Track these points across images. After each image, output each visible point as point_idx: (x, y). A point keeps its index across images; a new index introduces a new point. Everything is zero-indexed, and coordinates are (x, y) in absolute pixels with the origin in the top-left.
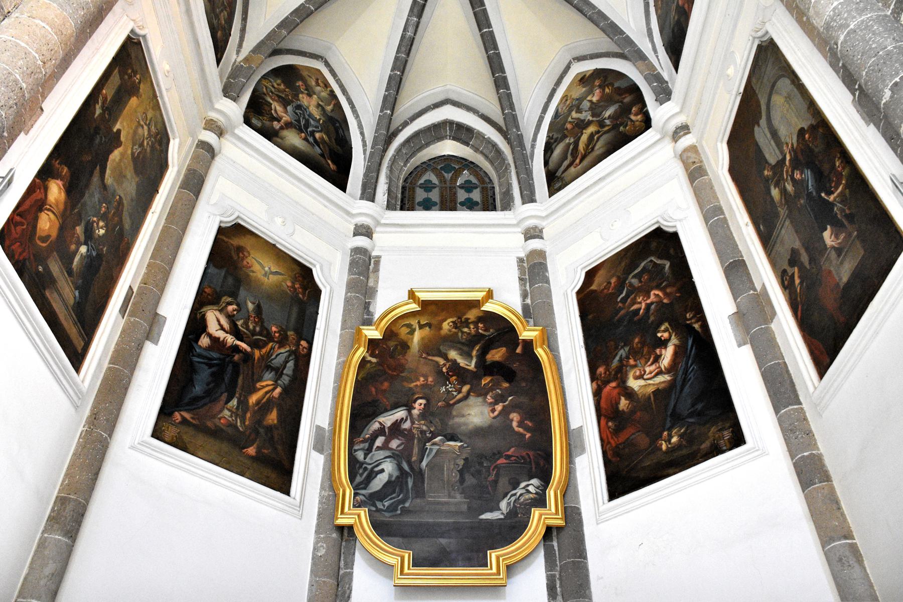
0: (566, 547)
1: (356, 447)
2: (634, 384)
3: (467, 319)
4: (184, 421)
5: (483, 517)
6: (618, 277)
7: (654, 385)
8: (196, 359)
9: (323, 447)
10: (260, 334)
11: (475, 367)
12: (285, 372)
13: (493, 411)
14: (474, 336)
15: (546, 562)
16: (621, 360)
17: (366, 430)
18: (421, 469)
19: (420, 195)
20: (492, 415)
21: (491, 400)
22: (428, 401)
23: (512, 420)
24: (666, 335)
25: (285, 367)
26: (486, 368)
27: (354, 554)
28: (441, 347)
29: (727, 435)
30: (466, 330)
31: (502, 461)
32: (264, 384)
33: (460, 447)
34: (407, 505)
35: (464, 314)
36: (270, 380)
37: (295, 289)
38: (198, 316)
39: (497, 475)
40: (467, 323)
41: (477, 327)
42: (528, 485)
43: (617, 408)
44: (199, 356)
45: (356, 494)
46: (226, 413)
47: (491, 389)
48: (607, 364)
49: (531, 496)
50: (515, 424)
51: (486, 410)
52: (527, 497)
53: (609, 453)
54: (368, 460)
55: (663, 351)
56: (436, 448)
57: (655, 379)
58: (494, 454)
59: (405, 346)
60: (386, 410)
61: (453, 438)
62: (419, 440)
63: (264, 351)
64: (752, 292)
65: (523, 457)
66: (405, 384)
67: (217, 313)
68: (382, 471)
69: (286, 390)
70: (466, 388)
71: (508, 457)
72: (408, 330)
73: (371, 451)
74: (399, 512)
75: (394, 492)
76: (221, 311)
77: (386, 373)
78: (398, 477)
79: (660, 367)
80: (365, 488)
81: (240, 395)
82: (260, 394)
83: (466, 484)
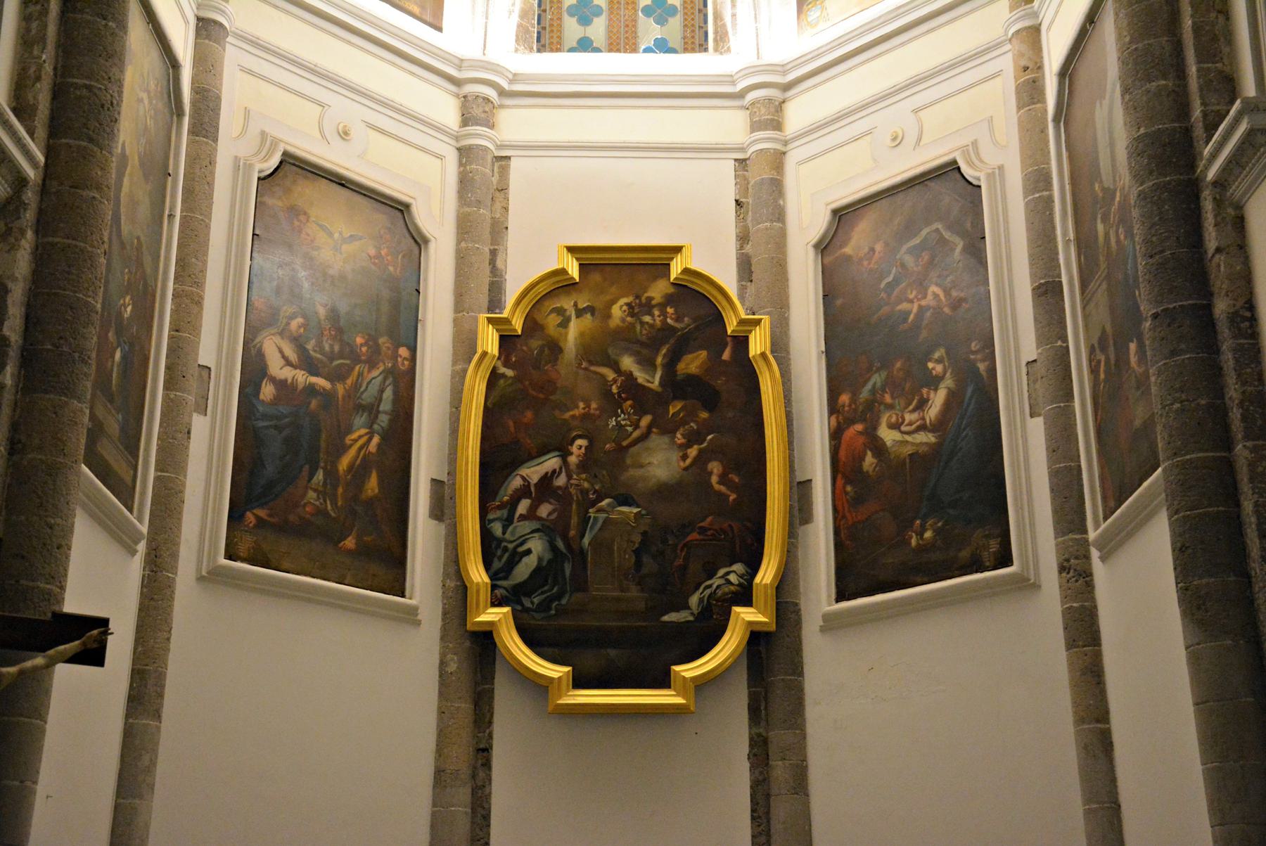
0: (771, 657)
1: (491, 516)
2: (888, 436)
3: (650, 299)
4: (261, 523)
5: (666, 618)
6: (887, 244)
7: (913, 444)
9: (442, 512)
10: (341, 356)
11: (661, 384)
13: (684, 457)
16: (873, 391)
19: (572, 29)
21: (683, 441)
23: (711, 473)
24: (939, 368)
25: (381, 400)
26: (676, 386)
28: (610, 351)
29: (994, 545)
30: (647, 319)
31: (695, 536)
32: (354, 436)
34: (564, 601)
35: (645, 290)
38: (253, 352)
39: (686, 559)
40: (648, 307)
42: (728, 573)
44: (265, 417)
45: (494, 587)
46: (312, 495)
47: (683, 422)
48: (855, 395)
49: (732, 588)
50: (714, 479)
51: (675, 456)
52: (726, 590)
54: (507, 536)
55: (932, 395)
56: (603, 516)
57: (916, 435)
58: (684, 526)
59: (555, 348)
60: (531, 457)
61: (626, 501)
62: (578, 503)
63: (349, 382)
64: (1059, 343)
65: (725, 532)
66: (557, 413)
67: (278, 339)
68: (529, 552)
69: (385, 437)
70: (646, 421)
71: (703, 530)
73: (512, 523)
76: (281, 334)
78: (550, 562)
79: (923, 419)
80: (506, 578)
81: (326, 463)
82: (352, 452)
83: (645, 571)
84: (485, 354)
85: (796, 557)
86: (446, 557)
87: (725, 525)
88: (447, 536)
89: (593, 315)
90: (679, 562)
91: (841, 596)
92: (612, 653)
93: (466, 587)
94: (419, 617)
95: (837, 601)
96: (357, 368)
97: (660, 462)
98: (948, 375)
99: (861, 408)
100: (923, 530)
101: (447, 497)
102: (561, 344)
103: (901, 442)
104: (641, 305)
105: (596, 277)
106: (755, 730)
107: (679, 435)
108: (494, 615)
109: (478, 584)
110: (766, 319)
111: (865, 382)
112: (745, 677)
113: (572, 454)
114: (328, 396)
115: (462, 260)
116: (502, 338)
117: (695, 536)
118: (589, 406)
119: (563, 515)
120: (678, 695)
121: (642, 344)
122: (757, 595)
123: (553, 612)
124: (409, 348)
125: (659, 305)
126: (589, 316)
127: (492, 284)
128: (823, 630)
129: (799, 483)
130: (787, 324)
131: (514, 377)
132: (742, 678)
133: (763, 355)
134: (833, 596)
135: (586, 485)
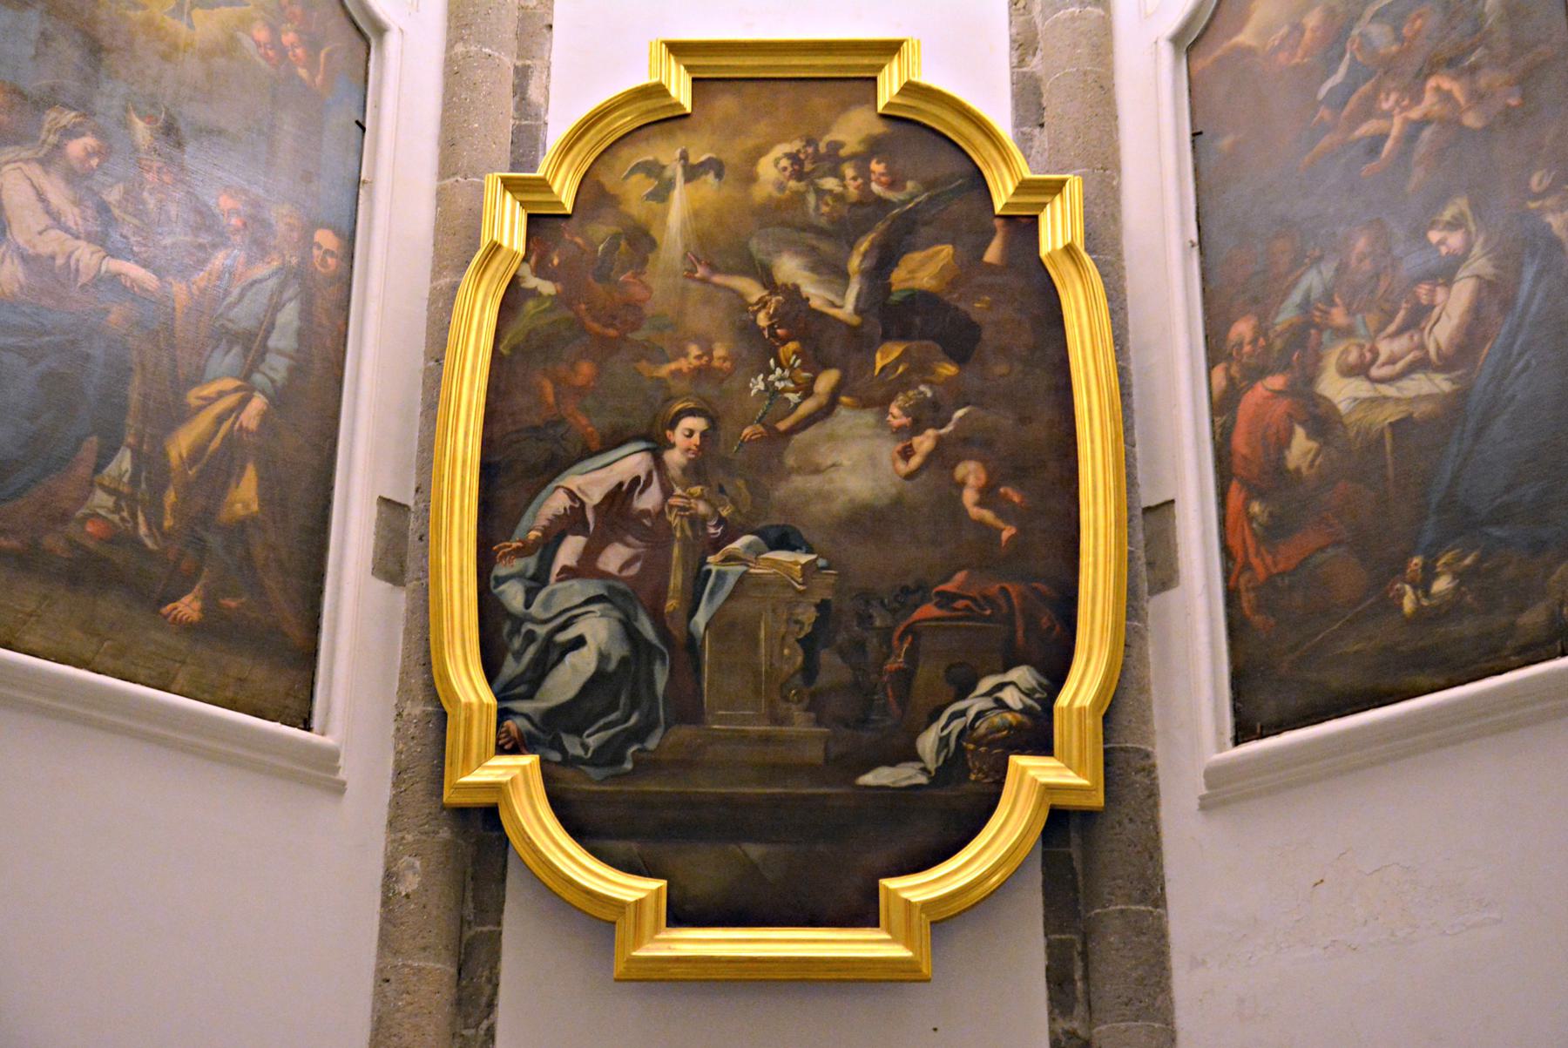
1: (501, 570)
2: (1338, 390)
3: (836, 146)
5: (868, 779)
7: (1398, 400)
9: (402, 564)
11: (858, 311)
12: (271, 343)
13: (907, 453)
14: (859, 204)
15: (1048, 904)
18: (691, 637)
20: (903, 468)
21: (904, 421)
22: (713, 422)
23: (961, 485)
26: (893, 314)
27: (503, 879)
28: (755, 245)
30: (830, 183)
31: (929, 610)
32: (209, 390)
33: (804, 566)
34: (652, 743)
35: (827, 129)
37: (282, 52)
39: (912, 655)
40: (833, 161)
41: (864, 174)
42: (1001, 687)
43: (1281, 459)
45: (503, 714)
46: (102, 500)
47: (904, 384)
49: (1009, 717)
50: (969, 497)
51: (888, 449)
52: (997, 720)
53: (1247, 600)
56: (735, 570)
58: (905, 590)
59: (640, 240)
60: (588, 453)
61: (784, 540)
67: (35, 171)
68: (580, 642)
69: (279, 400)
70: (826, 381)
71: (946, 599)
72: (650, 185)
73: (545, 583)
74: (628, 766)
75: (616, 709)
76: (45, 163)
77: (584, 330)
78: (623, 661)
79: (1422, 346)
80: (530, 696)
83: (823, 680)
84: (495, 248)
85: (1143, 660)
86: (407, 656)
87: (994, 589)
88: (411, 611)
89: (719, 175)
90: (896, 662)
91: (1243, 734)
92: (755, 851)
93: (443, 716)
94: (342, 776)
95: (1237, 742)
97: (856, 462)
98: (1477, 250)
99: (1278, 344)
100: (1429, 574)
101: (413, 538)
102: (654, 233)
103: (1372, 400)
104: (817, 158)
105: (725, 104)
106: (1063, 1025)
107: (894, 409)
108: (515, 777)
109: (469, 705)
110: (1075, 185)
111: (1286, 294)
112: (1038, 899)
113: (673, 446)
115: (455, 74)
116: (532, 220)
117: (929, 610)
119: (655, 565)
120: (896, 891)
121: (820, 232)
122: (1062, 731)
124: (338, 233)
125: (852, 157)
126: (710, 177)
127: (518, 131)
128: (1206, 805)
129: (1147, 510)
130: (1117, 201)
131: (558, 295)
132: (1032, 902)
133: (1069, 249)
134: (1229, 732)
135: (702, 508)
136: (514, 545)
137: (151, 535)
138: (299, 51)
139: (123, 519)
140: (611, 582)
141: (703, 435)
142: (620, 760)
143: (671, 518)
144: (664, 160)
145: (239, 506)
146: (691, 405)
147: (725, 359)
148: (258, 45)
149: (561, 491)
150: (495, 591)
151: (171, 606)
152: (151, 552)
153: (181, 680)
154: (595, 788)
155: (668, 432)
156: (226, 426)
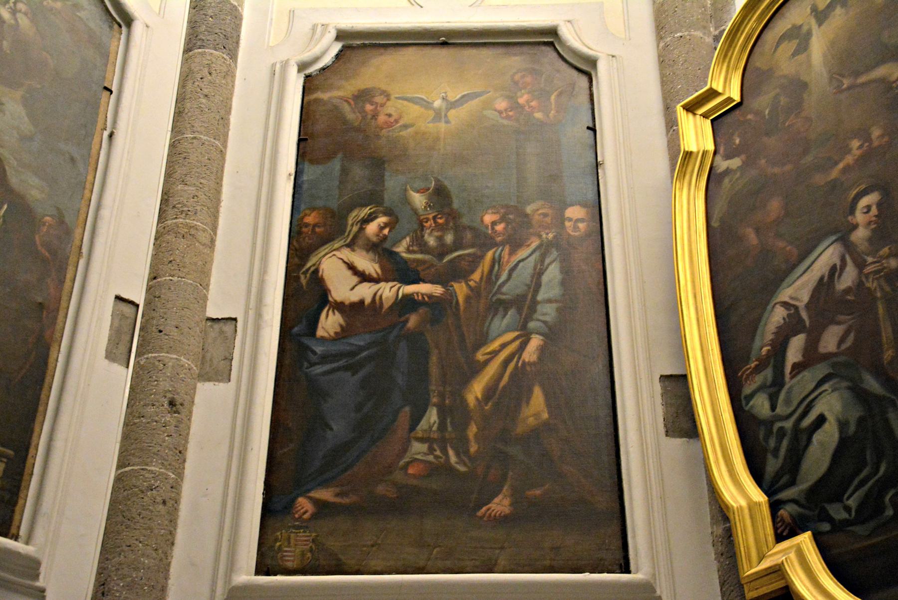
1: (747, 390)
4: (322, 508)
8: (319, 369)
17: (758, 338)
25: (538, 286)
32: (495, 345)
36: (508, 330)
44: (325, 359)
45: (775, 507)
63: (476, 276)
67: (346, 254)
68: (821, 420)
75: (864, 464)
76: (351, 245)
78: (861, 421)
80: (792, 483)
81: (442, 395)
96: (489, 255)
114: (437, 308)
118: (868, 139)
123: (890, 512)
136: (753, 365)
137: (461, 462)
138: (533, 104)
139: (436, 457)
140: (835, 359)
141: (879, 205)
142: (881, 509)
143: (868, 285)
144: (799, 22)
145: (531, 419)
146: (863, 187)
147: (882, 136)
148: (500, 112)
149: (777, 306)
150: (747, 409)
151: (484, 509)
152: (464, 474)
153: (502, 562)
154: (866, 543)
155: (850, 218)
156: (512, 366)
